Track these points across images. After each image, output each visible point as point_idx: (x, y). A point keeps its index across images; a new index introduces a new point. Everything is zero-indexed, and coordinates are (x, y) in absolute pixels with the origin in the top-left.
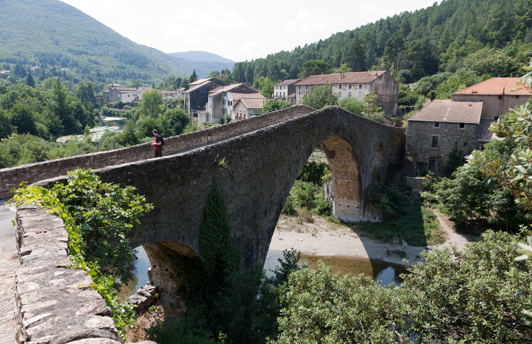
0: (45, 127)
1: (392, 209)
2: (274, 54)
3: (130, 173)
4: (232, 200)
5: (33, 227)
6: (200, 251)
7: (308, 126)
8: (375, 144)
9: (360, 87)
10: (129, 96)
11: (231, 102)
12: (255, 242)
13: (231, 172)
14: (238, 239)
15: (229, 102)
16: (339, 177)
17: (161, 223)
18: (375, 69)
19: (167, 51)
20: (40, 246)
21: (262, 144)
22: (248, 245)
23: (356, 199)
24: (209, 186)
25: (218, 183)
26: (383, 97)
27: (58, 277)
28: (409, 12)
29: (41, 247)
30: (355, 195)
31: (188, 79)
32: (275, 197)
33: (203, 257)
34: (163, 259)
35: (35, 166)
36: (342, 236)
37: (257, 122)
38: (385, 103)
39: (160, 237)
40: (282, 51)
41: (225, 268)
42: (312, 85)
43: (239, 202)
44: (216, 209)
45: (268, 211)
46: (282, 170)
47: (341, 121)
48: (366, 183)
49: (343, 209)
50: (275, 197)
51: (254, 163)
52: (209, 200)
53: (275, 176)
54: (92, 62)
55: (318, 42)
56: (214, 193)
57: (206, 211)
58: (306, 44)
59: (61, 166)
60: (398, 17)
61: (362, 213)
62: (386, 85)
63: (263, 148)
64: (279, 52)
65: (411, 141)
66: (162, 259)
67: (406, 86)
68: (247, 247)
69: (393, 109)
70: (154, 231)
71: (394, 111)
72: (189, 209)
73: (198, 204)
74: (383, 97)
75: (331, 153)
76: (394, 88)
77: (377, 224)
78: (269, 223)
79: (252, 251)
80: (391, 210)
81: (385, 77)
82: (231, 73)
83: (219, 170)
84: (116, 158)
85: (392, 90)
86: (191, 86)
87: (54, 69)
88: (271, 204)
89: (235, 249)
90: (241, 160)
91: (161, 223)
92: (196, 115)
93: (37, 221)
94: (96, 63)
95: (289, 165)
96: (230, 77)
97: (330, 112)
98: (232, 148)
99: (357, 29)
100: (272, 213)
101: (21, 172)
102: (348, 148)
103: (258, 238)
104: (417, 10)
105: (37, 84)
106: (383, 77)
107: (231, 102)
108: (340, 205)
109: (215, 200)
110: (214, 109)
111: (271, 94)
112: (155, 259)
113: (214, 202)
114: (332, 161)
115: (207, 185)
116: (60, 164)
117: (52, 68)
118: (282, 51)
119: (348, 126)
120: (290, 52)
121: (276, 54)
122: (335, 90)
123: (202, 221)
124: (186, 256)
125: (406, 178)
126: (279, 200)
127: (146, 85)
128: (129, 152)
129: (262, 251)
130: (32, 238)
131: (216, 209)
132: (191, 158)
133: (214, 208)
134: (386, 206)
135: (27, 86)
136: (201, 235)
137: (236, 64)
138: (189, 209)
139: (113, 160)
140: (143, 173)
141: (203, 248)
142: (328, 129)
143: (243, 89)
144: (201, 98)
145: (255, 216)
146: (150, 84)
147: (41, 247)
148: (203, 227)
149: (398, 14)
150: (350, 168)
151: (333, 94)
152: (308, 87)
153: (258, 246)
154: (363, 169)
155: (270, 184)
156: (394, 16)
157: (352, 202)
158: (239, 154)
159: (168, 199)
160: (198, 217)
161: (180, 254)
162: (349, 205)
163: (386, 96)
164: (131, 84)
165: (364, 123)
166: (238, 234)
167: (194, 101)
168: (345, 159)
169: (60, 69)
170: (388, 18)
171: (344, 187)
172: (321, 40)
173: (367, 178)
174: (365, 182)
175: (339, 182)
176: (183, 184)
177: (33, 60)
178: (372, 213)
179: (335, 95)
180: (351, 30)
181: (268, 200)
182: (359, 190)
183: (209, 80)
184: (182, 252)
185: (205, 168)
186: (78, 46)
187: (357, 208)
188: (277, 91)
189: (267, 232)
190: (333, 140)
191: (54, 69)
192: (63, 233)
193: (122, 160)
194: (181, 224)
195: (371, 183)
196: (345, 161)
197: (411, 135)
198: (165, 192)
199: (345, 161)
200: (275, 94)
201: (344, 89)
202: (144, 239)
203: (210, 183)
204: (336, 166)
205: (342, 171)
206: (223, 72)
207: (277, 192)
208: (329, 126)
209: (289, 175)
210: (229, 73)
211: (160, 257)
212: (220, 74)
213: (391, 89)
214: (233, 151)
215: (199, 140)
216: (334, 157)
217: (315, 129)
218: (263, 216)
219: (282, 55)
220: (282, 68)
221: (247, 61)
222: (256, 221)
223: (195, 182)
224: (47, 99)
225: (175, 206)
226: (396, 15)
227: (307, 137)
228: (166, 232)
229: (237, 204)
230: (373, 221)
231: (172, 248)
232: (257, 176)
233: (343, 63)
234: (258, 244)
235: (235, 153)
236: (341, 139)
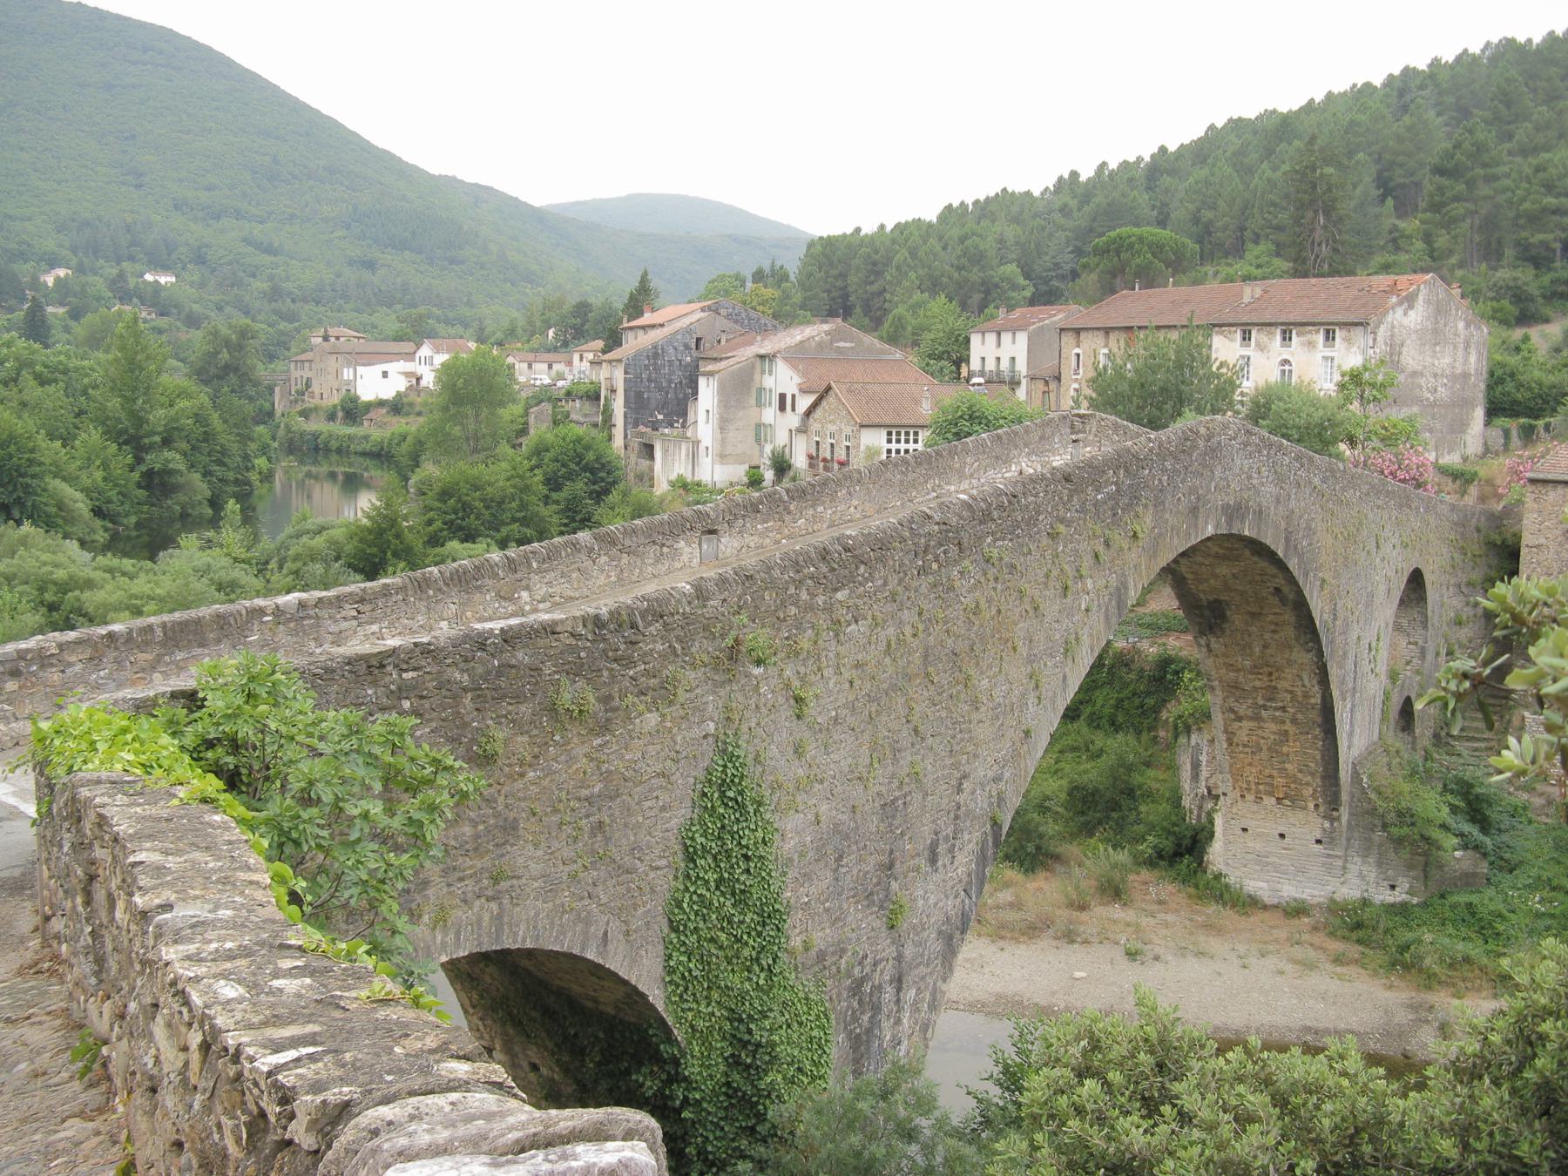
0: (78, 495)
1: (1465, 847)
2: (969, 201)
3: (411, 675)
4: (799, 799)
5: (151, 837)
6: (668, 998)
7: (1110, 497)
8: (1391, 574)
9: (1327, 338)
10: (385, 375)
11: (794, 396)
12: (887, 971)
13: (796, 683)
14: (821, 956)
15: (782, 397)
16: (1241, 713)
17: (519, 878)
18: (1386, 268)
19: (538, 194)
20: (192, 892)
21: (923, 571)
22: (860, 982)
23: (1311, 806)
24: (705, 737)
25: (744, 728)
26: (1422, 381)
27: (291, 973)
28: (1521, 39)
29: (196, 898)
30: (1310, 790)
31: (620, 306)
32: (973, 793)
33: (679, 1020)
34: (520, 1023)
35: (79, 642)
36: (1252, 961)
37: (902, 482)
38: (1433, 405)
39: (516, 934)
40: (1005, 190)
41: (766, 1072)
42: (1129, 329)
43: (824, 807)
44: (732, 834)
45: (942, 848)
46: (1001, 678)
47: (1249, 477)
48: (1355, 740)
49: (1258, 846)
50: (973, 793)
51: (889, 645)
52: (705, 794)
53: (975, 704)
54: (259, 246)
55: (1152, 156)
56: (725, 766)
57: (693, 839)
58: (1104, 164)
59: (163, 644)
60: (1475, 59)
61: (1340, 863)
62: (1435, 332)
63: (923, 589)
64: (992, 194)
65: (1539, 563)
66: (517, 1023)
67: (1517, 334)
68: (856, 989)
69: (1463, 431)
70: (494, 906)
71: (1469, 440)
72: (626, 825)
73: (663, 809)
74: (1422, 381)
75: (1207, 613)
76: (1467, 346)
77: (1402, 910)
78: (947, 897)
79: (876, 1009)
80: (1458, 854)
81: (1428, 302)
82: (792, 277)
83: (748, 675)
84: (355, 618)
85: (1460, 352)
86: (630, 335)
87: (121, 276)
88: (957, 817)
89: (807, 999)
90: (837, 635)
91: (519, 878)
92: (648, 450)
93: (159, 820)
94: (270, 250)
95: (1030, 660)
96: (786, 296)
97: (1201, 443)
98: (799, 584)
99: (1310, 107)
100: (961, 858)
101: (30, 662)
102: (1278, 590)
103: (899, 958)
104: (1552, 33)
105: (57, 334)
106: (1421, 298)
107: (794, 396)
108: (1245, 830)
109: (731, 794)
110: (724, 424)
111: (959, 368)
112: (489, 1022)
113: (726, 805)
114: (1214, 645)
115: (697, 732)
116: (159, 632)
117: (115, 271)
118: (1005, 190)
119: (1278, 501)
120: (1036, 193)
121: (976, 202)
122: (1225, 349)
123: (676, 878)
124: (614, 1017)
125: (1523, 718)
126: (991, 804)
127: (452, 331)
128: (400, 597)
129: (916, 1009)
130: (159, 870)
131: (732, 834)
132: (641, 624)
133: (723, 827)
134: (1436, 834)
135: (22, 343)
136: (673, 935)
137: (811, 245)
138: (626, 825)
139: (345, 625)
140: (457, 676)
141: (678, 986)
142: (1194, 511)
143: (842, 344)
144: (670, 381)
145: (891, 866)
146: (465, 325)
147: (196, 898)
148: (679, 905)
149: (1475, 49)
150: (1289, 673)
151: (1214, 369)
152: (1112, 336)
153: (899, 990)
154: (1343, 682)
155: (954, 737)
156: (1459, 59)
157: (1296, 817)
158: (829, 609)
159: (545, 783)
160: (663, 862)
161: (589, 1004)
162: (1281, 829)
163: (1435, 375)
164: (396, 326)
165: (1343, 490)
166: (822, 937)
167: (639, 395)
168: (1267, 636)
169: (142, 275)
170: (1435, 63)
171: (1264, 755)
172: (1163, 149)
173: (1358, 716)
174: (1351, 734)
175: (1242, 736)
176: (605, 728)
177: (49, 244)
178: (1379, 864)
179: (1224, 370)
180: (1283, 109)
181: (945, 801)
182: (1326, 768)
183: (703, 310)
184: (596, 1001)
185: (693, 666)
186: (209, 188)
187: (1319, 842)
188: (985, 351)
189: (940, 933)
190: (1217, 556)
191: (121, 276)
192: (252, 861)
193: (375, 628)
194: (594, 884)
195: (1375, 737)
196: (1265, 647)
197: (1542, 541)
198: (536, 757)
199: (1265, 647)
200: (975, 364)
201: (1261, 348)
202: (458, 934)
203: (712, 725)
204: (1230, 666)
205: (1255, 689)
206: (759, 276)
207: (981, 771)
208: (1198, 499)
209: (1032, 700)
210: (784, 277)
211: (510, 1014)
212: (749, 285)
213: (1455, 347)
214: (804, 596)
215: (665, 550)
216: (1223, 630)
217: (1140, 509)
218: (923, 862)
219: (1003, 206)
220: (1003, 261)
221: (858, 230)
222: (894, 885)
223: (652, 719)
224: (90, 391)
225: (573, 810)
226: (1465, 51)
227: (1107, 544)
228: (537, 914)
229: (817, 816)
230: (1383, 896)
231: (558, 982)
232: (901, 700)
233: (1256, 242)
234: (898, 982)
235: (810, 608)
236: (1247, 552)
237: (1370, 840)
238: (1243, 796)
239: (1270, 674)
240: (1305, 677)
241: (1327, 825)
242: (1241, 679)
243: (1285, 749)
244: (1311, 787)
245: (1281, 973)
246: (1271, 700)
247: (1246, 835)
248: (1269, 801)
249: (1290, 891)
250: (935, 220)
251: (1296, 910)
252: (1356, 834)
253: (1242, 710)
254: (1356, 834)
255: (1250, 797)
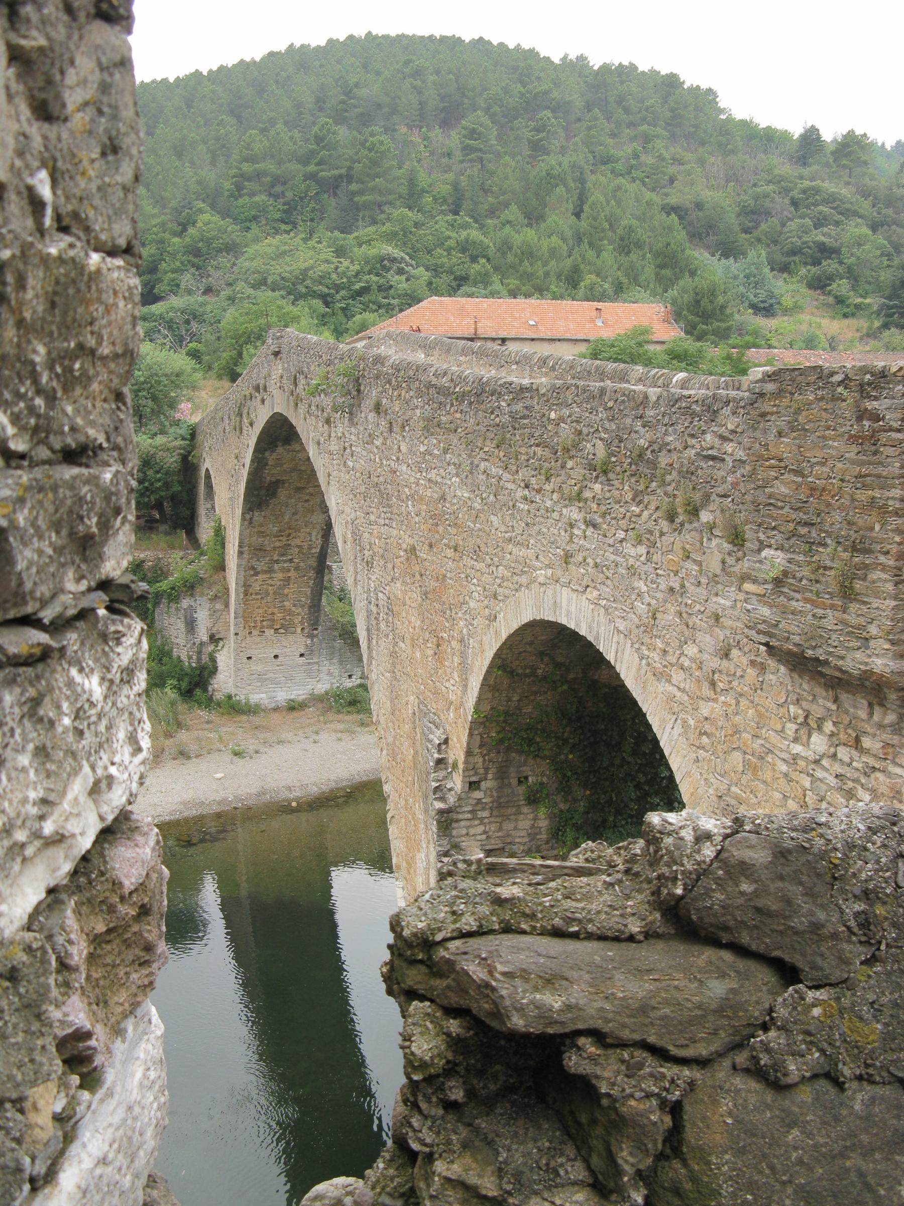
23: (299, 630)
108: (249, 658)
175: (256, 587)
178: (341, 662)
182: (312, 600)
187: (302, 655)
237: (332, 647)
238: (250, 633)
239: (289, 535)
240: (314, 534)
241: (309, 641)
242: (267, 542)
243: (286, 591)
244: (301, 614)
245: (340, 739)
246: (283, 555)
247: (250, 661)
248: (269, 632)
249: (282, 696)
250: (467, 41)
251: (293, 707)
252: (324, 645)
253: (260, 566)
254: (324, 645)
255: (255, 632)
